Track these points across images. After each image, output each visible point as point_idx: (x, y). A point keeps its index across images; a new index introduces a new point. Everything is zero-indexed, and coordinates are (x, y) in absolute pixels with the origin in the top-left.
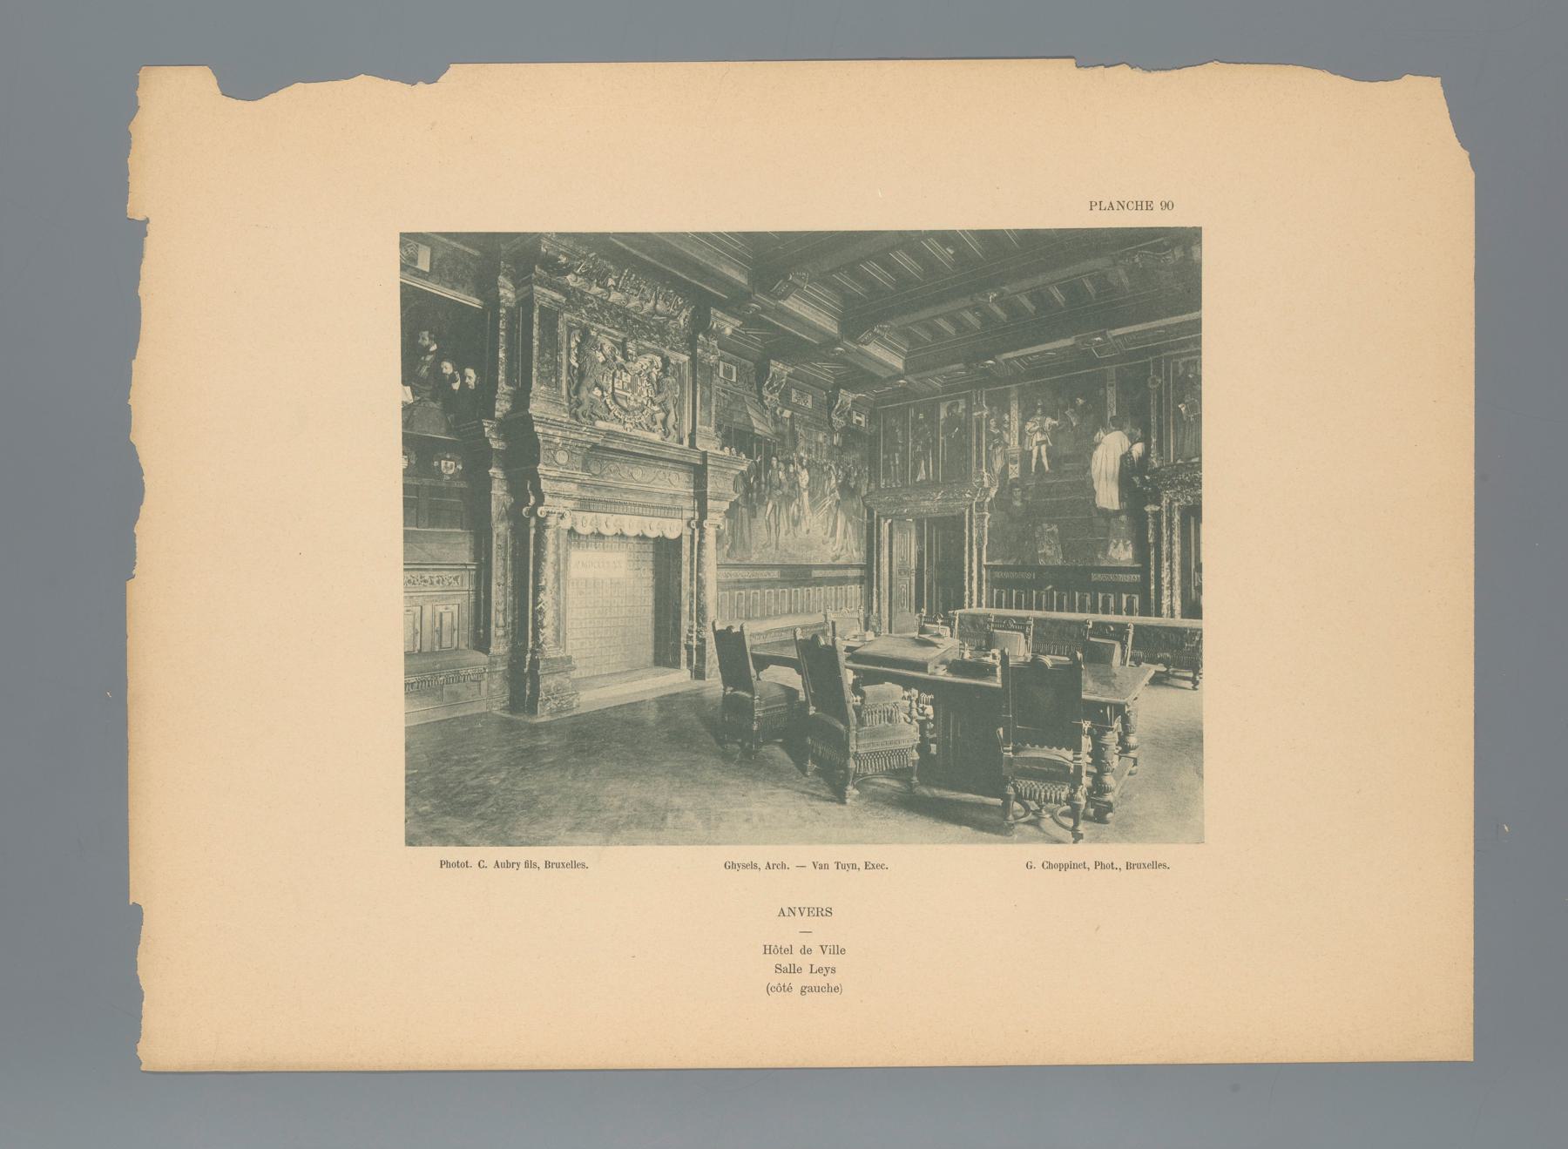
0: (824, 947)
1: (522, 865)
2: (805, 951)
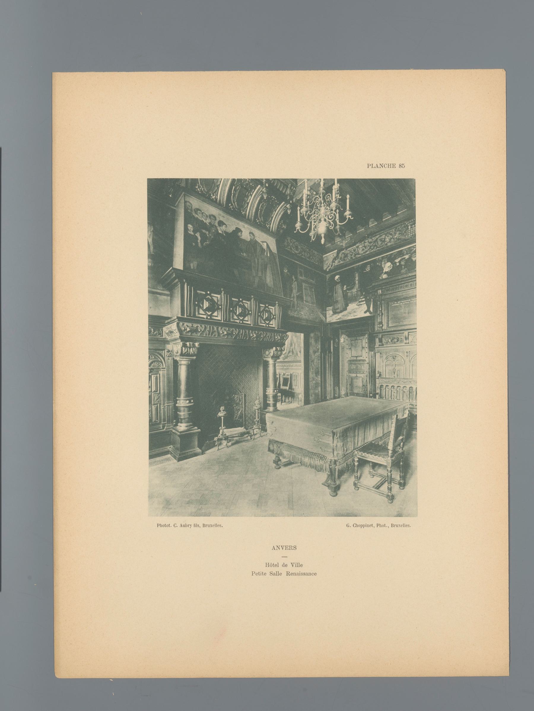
0: (293, 564)
1: (193, 526)
2: (285, 565)
